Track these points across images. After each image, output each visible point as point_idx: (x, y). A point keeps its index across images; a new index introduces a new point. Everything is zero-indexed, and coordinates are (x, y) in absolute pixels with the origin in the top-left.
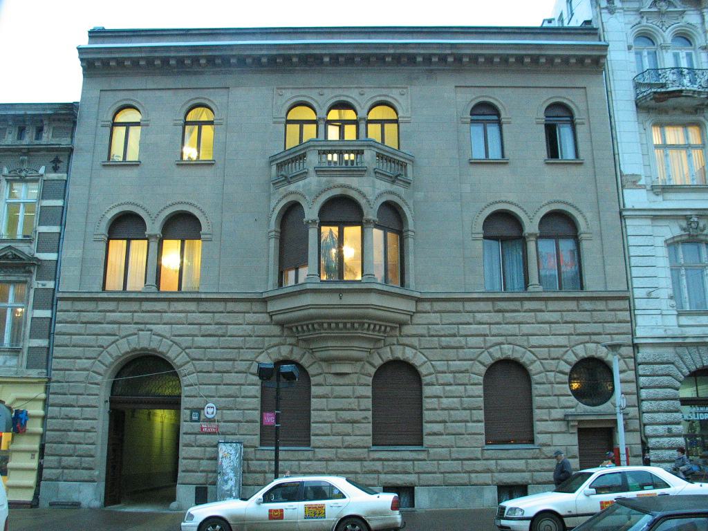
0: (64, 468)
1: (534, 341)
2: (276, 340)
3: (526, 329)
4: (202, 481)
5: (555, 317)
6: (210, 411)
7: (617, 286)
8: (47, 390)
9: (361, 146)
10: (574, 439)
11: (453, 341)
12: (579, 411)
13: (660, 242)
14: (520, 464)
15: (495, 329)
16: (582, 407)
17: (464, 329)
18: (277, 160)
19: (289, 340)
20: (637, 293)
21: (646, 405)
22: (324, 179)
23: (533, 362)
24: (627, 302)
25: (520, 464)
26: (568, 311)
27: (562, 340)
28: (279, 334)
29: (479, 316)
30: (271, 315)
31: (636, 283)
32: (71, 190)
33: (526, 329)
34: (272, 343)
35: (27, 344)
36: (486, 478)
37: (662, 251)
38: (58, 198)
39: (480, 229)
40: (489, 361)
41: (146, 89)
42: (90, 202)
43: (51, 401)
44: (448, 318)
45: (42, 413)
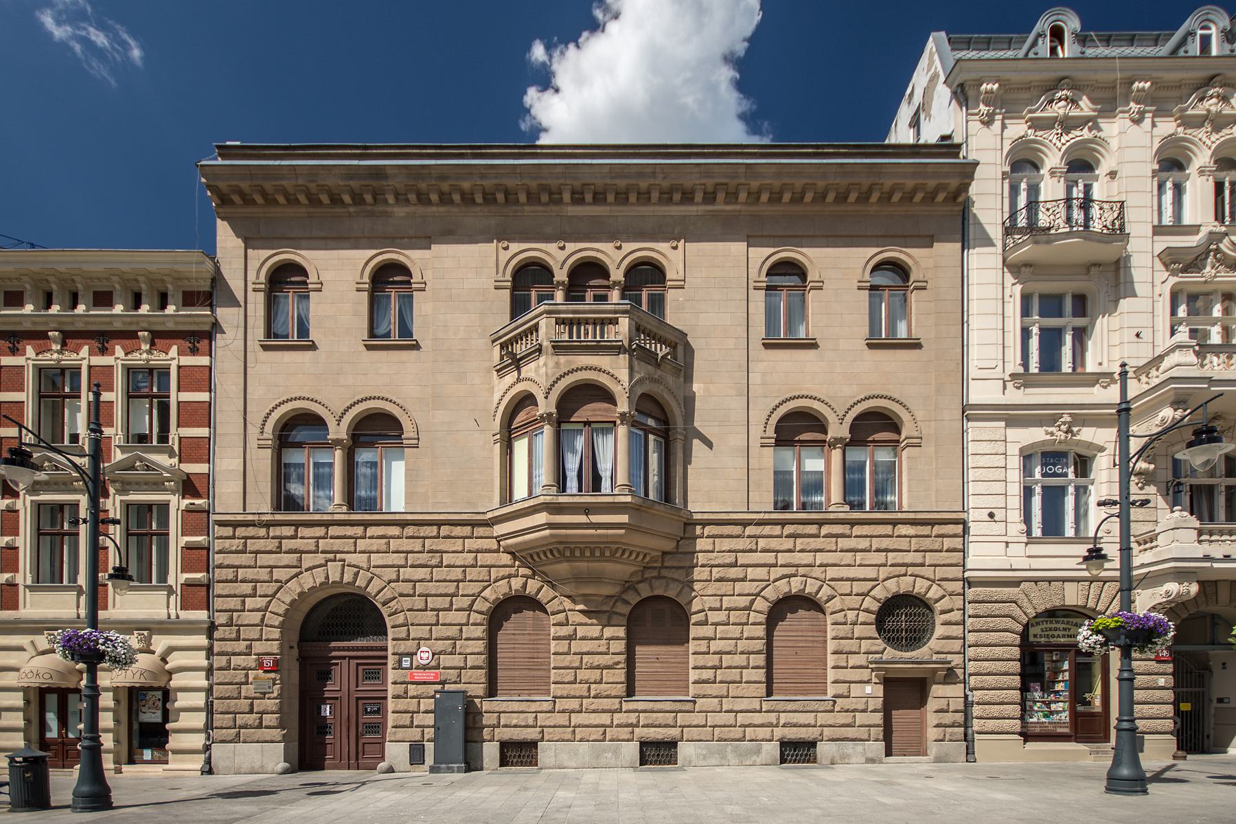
0: (241, 727)
1: (832, 572)
2: (506, 571)
3: (820, 558)
4: (418, 738)
5: (864, 543)
6: (425, 655)
7: (946, 505)
8: (210, 637)
9: (616, 312)
10: (880, 690)
11: (734, 573)
12: (885, 658)
13: (1014, 450)
14: (808, 718)
15: (783, 559)
16: (890, 653)
17: (743, 559)
18: (500, 338)
19: (523, 571)
20: (973, 515)
21: (971, 652)
22: (562, 359)
23: (525, 585)
24: (961, 526)
25: (808, 718)
26: (880, 536)
27: (870, 573)
28: (509, 563)
29: (762, 543)
30: (499, 539)
31: (972, 502)
32: (217, 377)
33: (820, 558)
34: (501, 575)
35: (985, 555)
36: (764, 732)
37: (1015, 462)
38: (199, 389)
39: (771, 432)
40: (875, 606)
41: (311, 238)
42: (168, 706)
43: (216, 649)
44: (727, 544)
45: (205, 663)
